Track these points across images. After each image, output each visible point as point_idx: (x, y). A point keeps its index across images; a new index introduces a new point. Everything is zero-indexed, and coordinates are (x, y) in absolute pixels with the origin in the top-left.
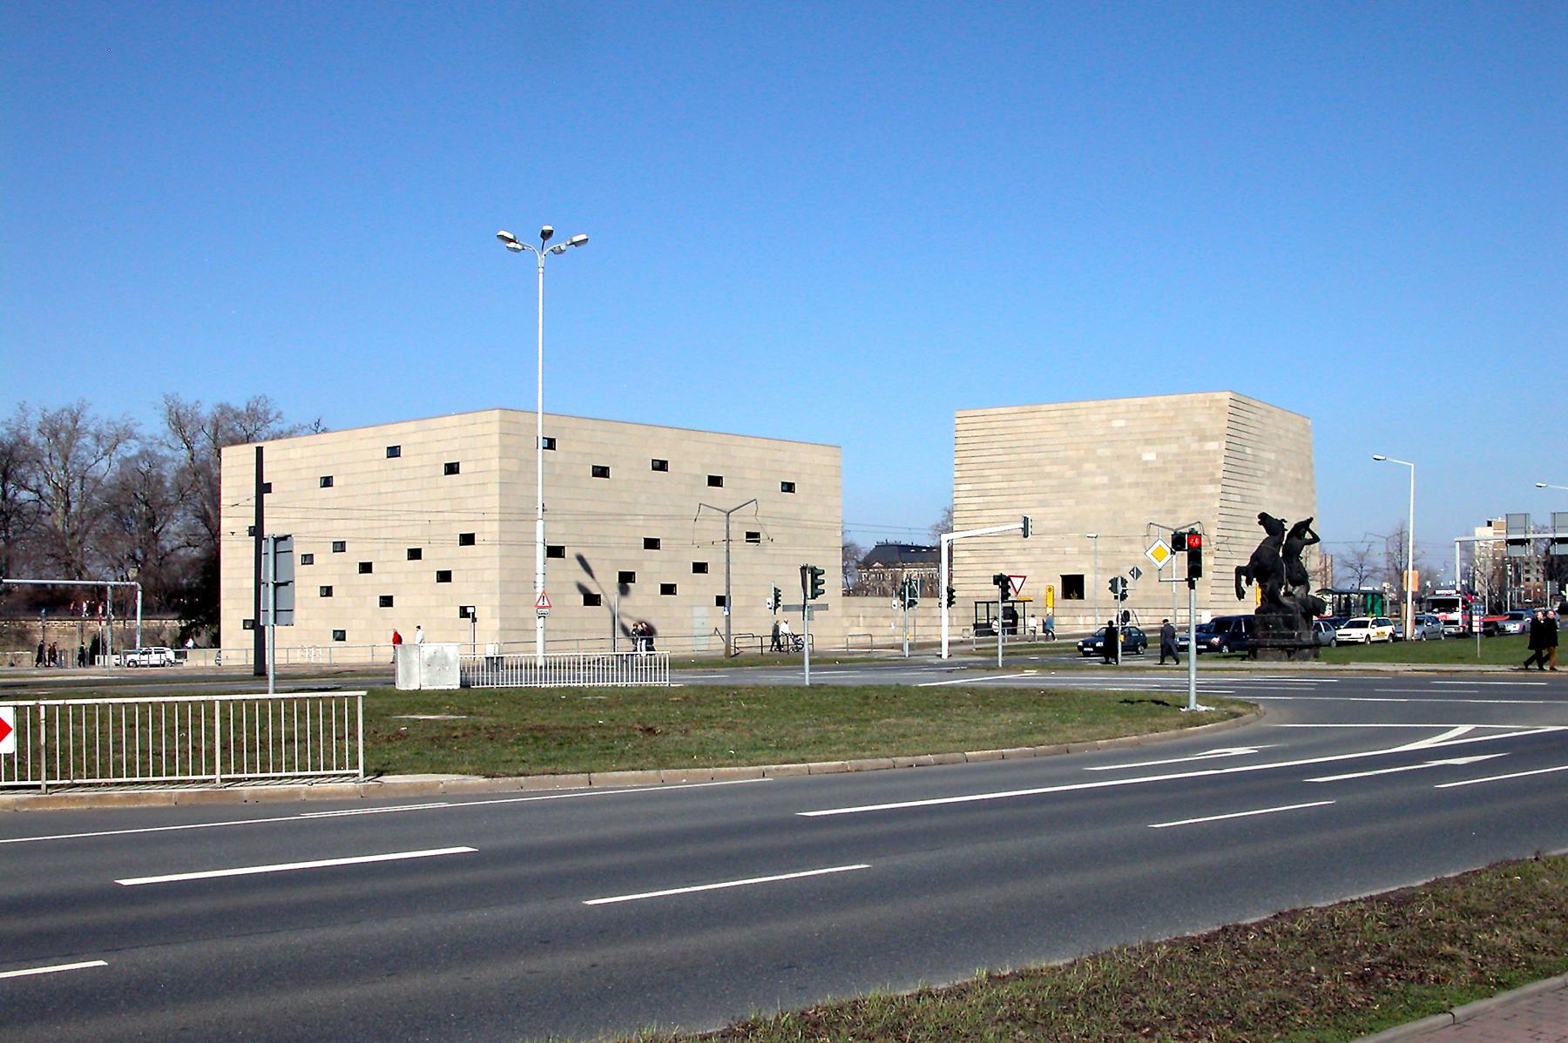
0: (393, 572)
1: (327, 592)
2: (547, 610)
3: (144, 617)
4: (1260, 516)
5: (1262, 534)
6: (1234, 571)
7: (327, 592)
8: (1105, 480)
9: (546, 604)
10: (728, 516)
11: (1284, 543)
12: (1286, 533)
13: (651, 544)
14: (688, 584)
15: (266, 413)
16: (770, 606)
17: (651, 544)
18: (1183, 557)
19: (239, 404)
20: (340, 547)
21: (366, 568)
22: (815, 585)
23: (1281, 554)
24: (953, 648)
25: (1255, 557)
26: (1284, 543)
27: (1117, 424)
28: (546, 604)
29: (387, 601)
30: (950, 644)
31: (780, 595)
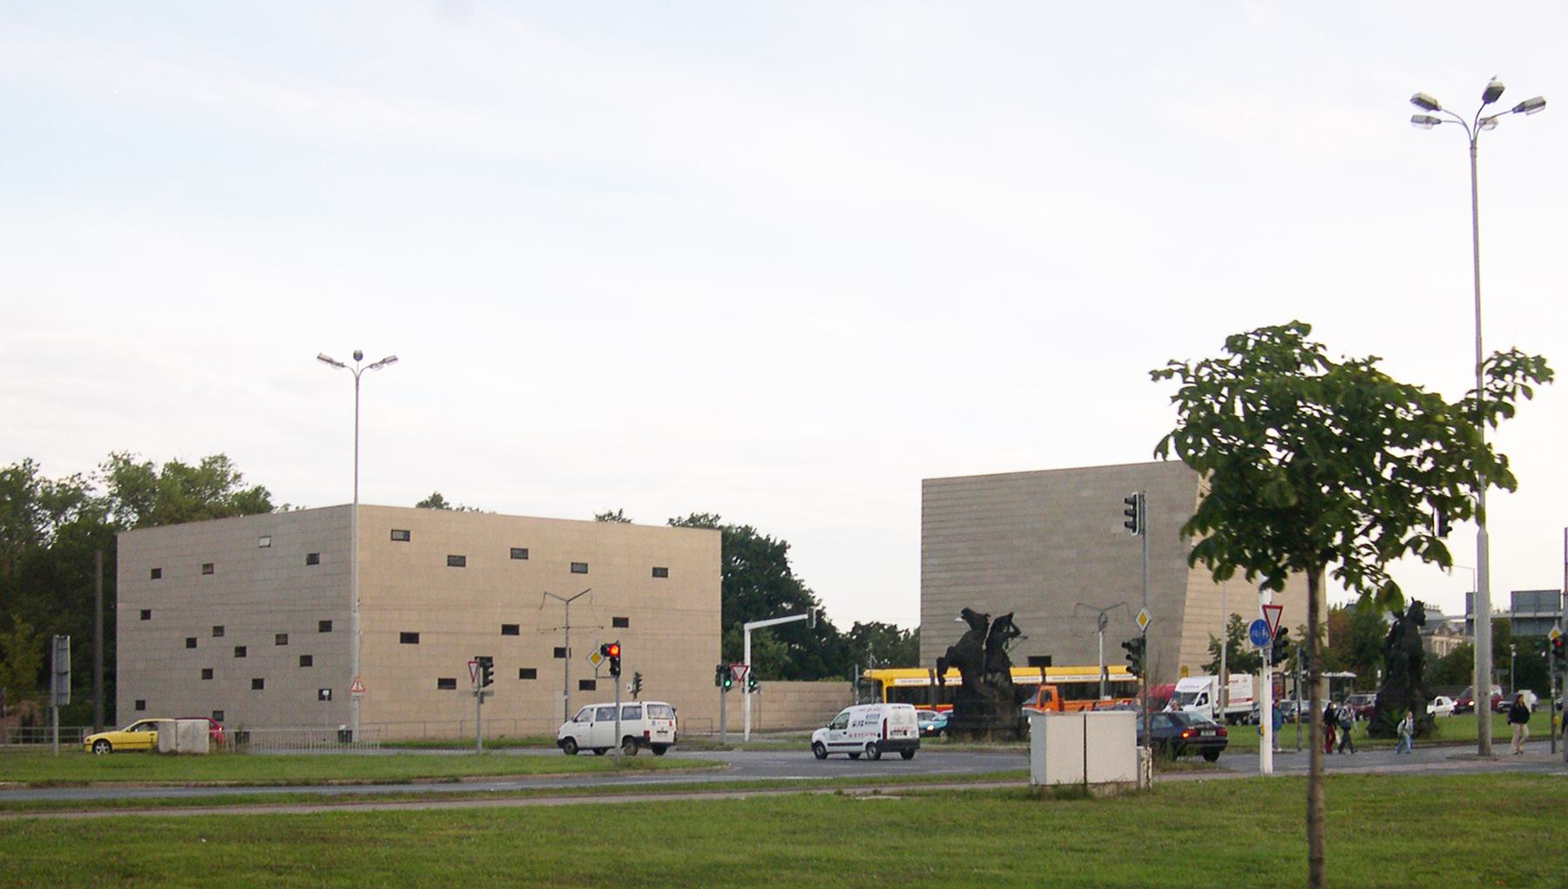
0: (263, 657)
1: (208, 674)
2: (360, 694)
3: (638, 710)
4: (963, 612)
5: (966, 627)
6: (936, 663)
7: (208, 674)
8: (1073, 554)
9: (360, 688)
10: (567, 604)
11: (987, 636)
12: (990, 626)
13: (510, 630)
14: (550, 670)
15: (225, 475)
16: (631, 690)
17: (510, 630)
18: (607, 663)
19: (194, 463)
20: (219, 631)
21: (241, 652)
22: (486, 675)
23: (984, 647)
24: (753, 734)
25: (950, 650)
26: (987, 636)
27: (1086, 493)
28: (360, 688)
29: (258, 684)
30: (751, 731)
31: (640, 680)
